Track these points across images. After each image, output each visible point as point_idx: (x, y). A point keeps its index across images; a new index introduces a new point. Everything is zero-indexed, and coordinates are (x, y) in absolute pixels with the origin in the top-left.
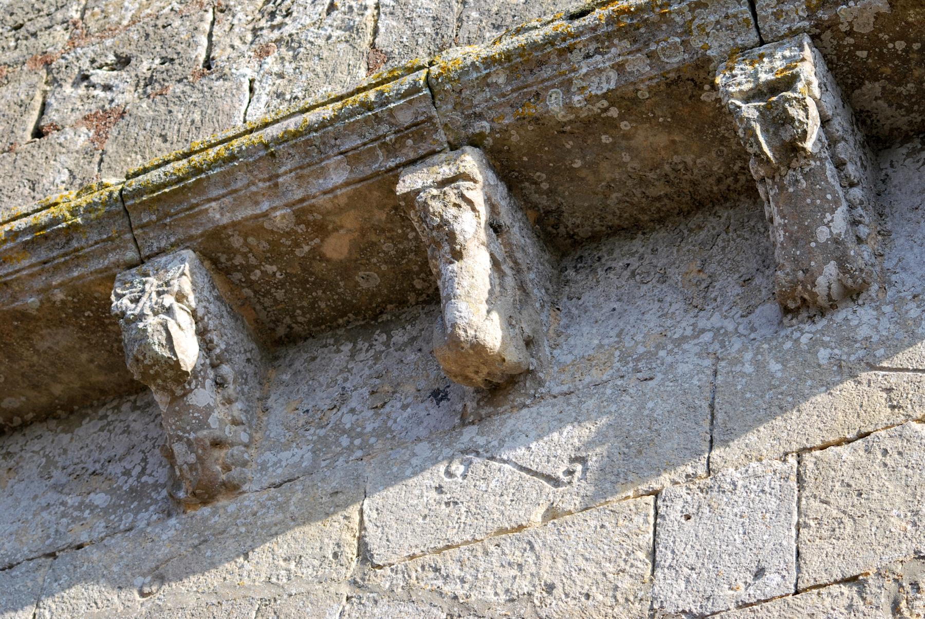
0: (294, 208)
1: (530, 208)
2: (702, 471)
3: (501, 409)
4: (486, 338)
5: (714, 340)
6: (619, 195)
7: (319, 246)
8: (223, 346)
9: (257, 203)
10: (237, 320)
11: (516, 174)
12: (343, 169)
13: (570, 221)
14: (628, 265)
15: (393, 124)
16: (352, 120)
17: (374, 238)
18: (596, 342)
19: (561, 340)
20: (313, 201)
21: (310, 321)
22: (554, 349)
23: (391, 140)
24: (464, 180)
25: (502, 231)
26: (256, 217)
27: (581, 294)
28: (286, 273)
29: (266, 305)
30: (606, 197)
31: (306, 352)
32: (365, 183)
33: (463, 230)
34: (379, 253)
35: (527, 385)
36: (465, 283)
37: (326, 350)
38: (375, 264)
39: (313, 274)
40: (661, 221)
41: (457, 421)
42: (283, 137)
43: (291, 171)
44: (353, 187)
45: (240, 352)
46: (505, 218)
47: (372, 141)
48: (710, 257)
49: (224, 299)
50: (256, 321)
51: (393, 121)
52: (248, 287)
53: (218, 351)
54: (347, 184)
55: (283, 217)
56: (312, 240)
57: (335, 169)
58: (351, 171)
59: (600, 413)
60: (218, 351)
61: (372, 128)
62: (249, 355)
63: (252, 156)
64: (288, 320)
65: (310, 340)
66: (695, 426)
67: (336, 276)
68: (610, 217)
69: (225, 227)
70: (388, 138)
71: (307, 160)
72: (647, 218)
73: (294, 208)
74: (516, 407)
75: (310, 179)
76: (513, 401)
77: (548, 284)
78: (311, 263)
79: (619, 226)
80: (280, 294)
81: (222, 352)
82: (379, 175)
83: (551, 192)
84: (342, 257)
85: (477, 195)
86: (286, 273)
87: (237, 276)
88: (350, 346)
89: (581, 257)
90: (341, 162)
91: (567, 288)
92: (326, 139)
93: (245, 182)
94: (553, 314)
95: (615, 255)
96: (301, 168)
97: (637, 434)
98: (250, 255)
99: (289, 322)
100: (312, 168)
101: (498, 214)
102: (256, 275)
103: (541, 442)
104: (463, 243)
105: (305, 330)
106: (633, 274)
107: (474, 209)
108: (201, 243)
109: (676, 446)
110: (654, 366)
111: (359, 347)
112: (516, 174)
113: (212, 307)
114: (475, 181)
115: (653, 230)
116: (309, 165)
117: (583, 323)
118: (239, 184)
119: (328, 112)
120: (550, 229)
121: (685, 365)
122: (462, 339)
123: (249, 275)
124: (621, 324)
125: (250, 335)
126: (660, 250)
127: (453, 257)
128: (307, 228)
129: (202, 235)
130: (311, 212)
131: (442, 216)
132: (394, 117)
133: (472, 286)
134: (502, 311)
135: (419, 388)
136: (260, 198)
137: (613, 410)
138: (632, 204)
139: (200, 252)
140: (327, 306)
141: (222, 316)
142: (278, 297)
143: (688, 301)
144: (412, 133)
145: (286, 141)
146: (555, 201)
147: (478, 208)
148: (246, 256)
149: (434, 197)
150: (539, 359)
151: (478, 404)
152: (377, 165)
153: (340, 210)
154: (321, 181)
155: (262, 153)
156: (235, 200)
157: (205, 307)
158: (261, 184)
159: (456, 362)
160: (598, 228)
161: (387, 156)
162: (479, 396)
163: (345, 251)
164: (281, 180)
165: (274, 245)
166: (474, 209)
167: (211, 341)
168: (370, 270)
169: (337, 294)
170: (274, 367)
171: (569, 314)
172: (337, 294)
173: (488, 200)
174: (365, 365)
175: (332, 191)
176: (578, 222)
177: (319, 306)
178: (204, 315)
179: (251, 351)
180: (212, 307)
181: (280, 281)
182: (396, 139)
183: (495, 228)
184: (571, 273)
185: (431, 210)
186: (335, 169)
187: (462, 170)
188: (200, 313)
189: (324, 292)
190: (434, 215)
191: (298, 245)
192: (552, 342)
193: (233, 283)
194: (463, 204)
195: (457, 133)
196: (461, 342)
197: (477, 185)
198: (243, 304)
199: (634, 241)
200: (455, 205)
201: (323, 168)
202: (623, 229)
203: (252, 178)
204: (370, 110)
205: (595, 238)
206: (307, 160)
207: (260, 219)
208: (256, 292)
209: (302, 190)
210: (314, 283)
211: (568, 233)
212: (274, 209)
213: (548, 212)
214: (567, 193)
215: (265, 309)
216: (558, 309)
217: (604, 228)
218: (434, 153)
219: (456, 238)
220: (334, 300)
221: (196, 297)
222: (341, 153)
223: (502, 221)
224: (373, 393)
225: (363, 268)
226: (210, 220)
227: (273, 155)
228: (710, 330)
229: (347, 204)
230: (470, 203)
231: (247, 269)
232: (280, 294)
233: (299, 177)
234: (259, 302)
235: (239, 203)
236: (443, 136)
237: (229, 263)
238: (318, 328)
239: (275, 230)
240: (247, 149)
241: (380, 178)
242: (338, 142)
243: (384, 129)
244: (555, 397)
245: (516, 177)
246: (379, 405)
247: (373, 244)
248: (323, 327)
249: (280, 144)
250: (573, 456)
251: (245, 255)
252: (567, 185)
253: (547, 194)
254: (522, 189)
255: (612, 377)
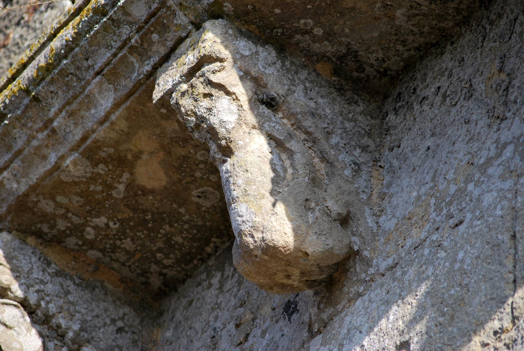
0: (81, 149)
1: (318, 61)
2: (507, 324)
3: (340, 307)
4: (274, 237)
5: (514, 153)
6: (404, 10)
7: (134, 180)
8: (76, 327)
9: (45, 158)
10: (94, 289)
11: (280, 30)
12: (109, 90)
13: (373, 58)
14: (439, 88)
15: (132, 23)
16: (92, 33)
17: (182, 152)
18: (415, 194)
19: (385, 203)
20: (94, 136)
21: (178, 262)
22: (380, 216)
23: (136, 41)
24: (210, 63)
25: (277, 103)
26: (50, 173)
27: (400, 140)
28: (119, 220)
29: (121, 260)
30: (392, 18)
31: (184, 297)
32: (132, 98)
33: (222, 122)
34: (197, 165)
35: (358, 269)
36: (240, 182)
37: (200, 288)
38: (202, 178)
39: (147, 211)
40: (465, 22)
41: (306, 334)
42: (37, 76)
43: (60, 111)
44: (124, 106)
45: (105, 324)
46: (276, 88)
47: (121, 48)
48: (509, 50)
49: (67, 271)
50: (123, 280)
51: (130, 19)
52: (92, 248)
53: (71, 334)
54: (117, 105)
55: (75, 163)
56: (121, 177)
57: (100, 93)
58: (116, 90)
59: (420, 281)
60: (71, 334)
61: (115, 34)
62: (120, 324)
63: (18, 108)
64: (154, 268)
65: (188, 281)
66: (499, 268)
67: (171, 204)
68: (411, 38)
69: (26, 195)
70: (133, 41)
71: (71, 93)
72: (451, 24)
73: (81, 149)
74: (352, 299)
75: (82, 113)
76: (348, 293)
77: (366, 141)
78: (137, 201)
79: (426, 44)
80: (128, 244)
81: (77, 334)
82: (142, 84)
83: (330, 35)
84: (164, 183)
85: (229, 76)
86: (119, 220)
87: (71, 241)
88: (219, 275)
89: (400, 94)
90: (100, 83)
91: (388, 138)
92: (78, 63)
93: (24, 138)
94: (375, 174)
95: (428, 80)
96: (68, 103)
97: (451, 296)
98: (70, 215)
99: (158, 269)
100: (80, 99)
101: (265, 86)
102: (90, 233)
103: (372, 336)
104: (227, 136)
105: (179, 272)
106: (445, 96)
107: (228, 93)
108: (12, 221)
109: (483, 299)
110: (464, 205)
111: (226, 273)
112: (280, 30)
113: (49, 288)
114: (221, 60)
115: (460, 35)
116: (75, 97)
117: (403, 175)
118: (20, 143)
119: (68, 33)
120: (355, 74)
121: (489, 195)
122: (252, 247)
123: (83, 236)
124: (435, 165)
125: (119, 299)
126: (466, 58)
127: (224, 155)
128: (107, 166)
129: (9, 212)
130: (99, 148)
131: (195, 113)
132: (129, 15)
133: (248, 182)
134: (291, 199)
135: (275, 305)
136: (45, 151)
137: (430, 274)
138: (424, 15)
139: (17, 230)
140: (184, 238)
141: (67, 293)
142: (128, 248)
143: (491, 113)
144: (152, 25)
145: (43, 79)
146: (340, 43)
147: (231, 89)
148: (67, 218)
149: (183, 94)
150: (360, 235)
151: (319, 308)
152: (136, 74)
153: (128, 136)
154: (93, 111)
155: (26, 101)
156: (23, 162)
157: (38, 291)
158: (40, 136)
159: (258, 273)
160: (406, 55)
161: (141, 59)
162: (318, 299)
163: (161, 174)
164: (55, 124)
165: (87, 196)
166: (228, 93)
167: (59, 326)
168: (201, 186)
169: (185, 223)
170: (159, 325)
171: (392, 171)
172: (185, 223)
173: (245, 76)
174: (231, 295)
175: (106, 118)
176: (380, 56)
177: (177, 242)
178: (39, 301)
179: (122, 319)
180: (49, 288)
181: (118, 231)
182: (141, 38)
183: (266, 102)
184: (391, 117)
185: (183, 110)
186: (100, 93)
187: (203, 52)
188: (33, 299)
189: (171, 226)
190: (188, 115)
191: (111, 187)
192: (376, 209)
193: (72, 250)
194: (214, 91)
195: (195, 10)
196: (252, 250)
197: (225, 64)
198: (97, 269)
199: (444, 56)
200: (206, 95)
201: (88, 96)
202: (433, 45)
203: (29, 132)
204: (105, 15)
205: (409, 67)
206: (71, 93)
207: (55, 174)
208: (103, 251)
209: (80, 127)
210: (154, 220)
211: (378, 72)
212: (62, 158)
213: (341, 58)
214: (347, 31)
215: (123, 264)
216: (380, 166)
217: (412, 52)
218: (181, 40)
219: (217, 133)
220: (187, 230)
221: (21, 285)
222: (98, 73)
223: (273, 93)
224: (237, 326)
225: (192, 186)
226: (10, 192)
227: (36, 99)
228: (511, 142)
229: (129, 127)
230: (220, 87)
231: (77, 230)
232: (128, 244)
233: (71, 114)
234: (112, 259)
235: (28, 165)
236: (184, 18)
237: (55, 231)
238: (191, 265)
239: (76, 180)
240: (10, 101)
241: (144, 87)
242: (90, 62)
243: (125, 31)
244: (383, 275)
245: (282, 34)
246: (242, 339)
247: (185, 158)
248: (195, 262)
249: (38, 84)
250: (398, 343)
251: (64, 217)
252: (341, 22)
253: (327, 39)
254: (297, 44)
255: (429, 232)
